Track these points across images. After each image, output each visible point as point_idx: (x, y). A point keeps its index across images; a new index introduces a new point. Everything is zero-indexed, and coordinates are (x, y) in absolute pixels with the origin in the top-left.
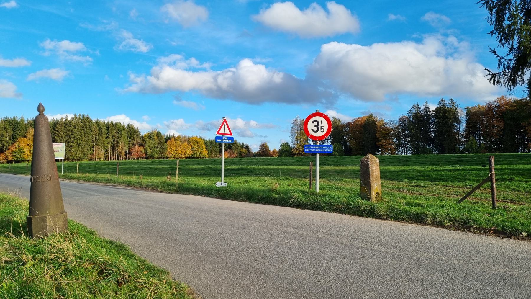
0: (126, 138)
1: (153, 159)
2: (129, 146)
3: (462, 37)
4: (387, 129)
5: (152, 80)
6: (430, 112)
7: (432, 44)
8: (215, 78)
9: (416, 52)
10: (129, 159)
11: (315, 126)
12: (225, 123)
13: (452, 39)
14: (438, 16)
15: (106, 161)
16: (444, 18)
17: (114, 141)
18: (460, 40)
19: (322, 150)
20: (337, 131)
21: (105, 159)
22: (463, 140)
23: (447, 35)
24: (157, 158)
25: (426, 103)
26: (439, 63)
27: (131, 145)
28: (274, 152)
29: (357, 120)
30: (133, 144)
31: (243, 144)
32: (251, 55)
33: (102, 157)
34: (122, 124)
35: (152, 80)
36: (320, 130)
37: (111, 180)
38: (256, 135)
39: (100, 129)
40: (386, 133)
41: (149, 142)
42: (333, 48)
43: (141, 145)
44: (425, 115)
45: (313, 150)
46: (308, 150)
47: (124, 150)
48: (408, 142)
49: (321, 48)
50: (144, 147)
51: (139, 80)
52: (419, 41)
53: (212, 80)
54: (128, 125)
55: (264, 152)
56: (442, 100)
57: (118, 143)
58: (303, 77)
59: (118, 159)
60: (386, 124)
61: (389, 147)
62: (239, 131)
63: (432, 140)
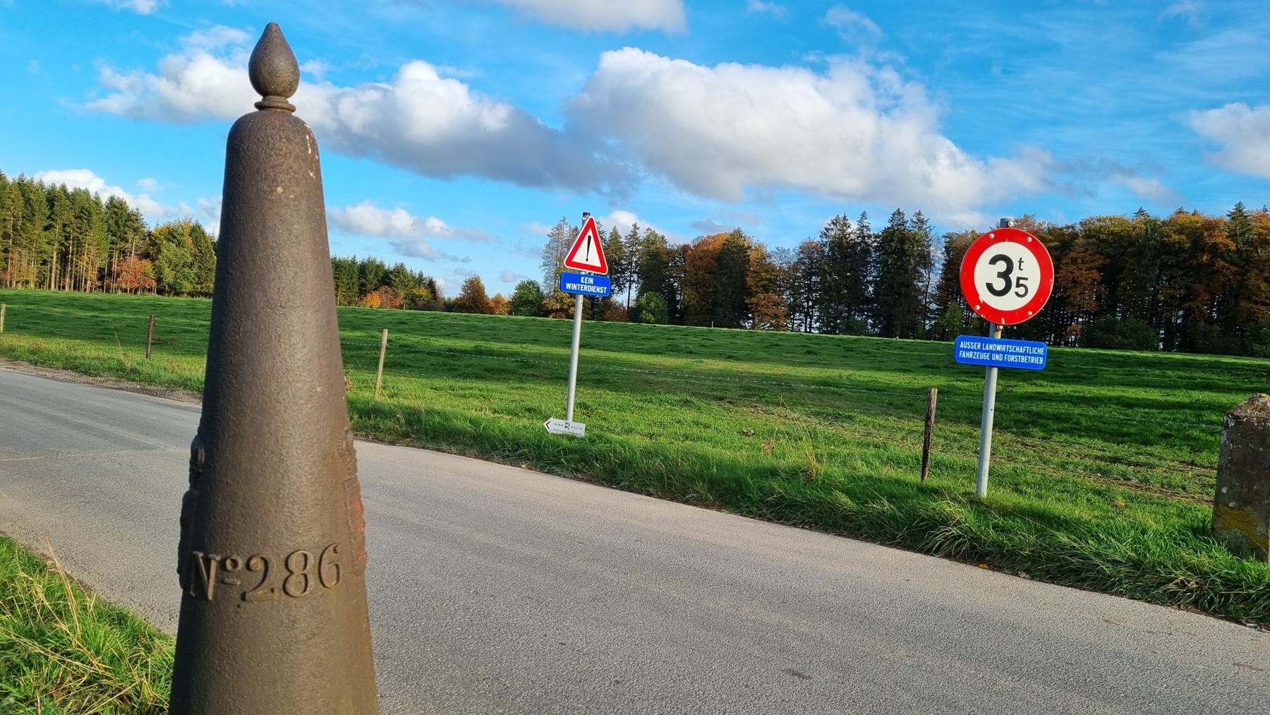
0: (104, 235)
1: (177, 294)
2: (111, 257)
3: (910, 71)
4: (770, 269)
5: (163, 86)
6: (869, 237)
7: (848, 81)
8: (334, 104)
9: (813, 93)
10: (108, 291)
11: (1000, 275)
12: (590, 233)
13: (889, 76)
14: (854, 16)
15: (43, 292)
16: (868, 23)
17: (67, 239)
18: (906, 79)
19: (1012, 358)
20: (655, 265)
21: (40, 284)
22: (933, 306)
23: (879, 66)
24: (191, 294)
25: (864, 216)
26: (864, 123)
27: (116, 254)
28: (497, 301)
29: (705, 243)
30: (123, 252)
31: (421, 275)
32: (441, 55)
33: (33, 279)
34: (92, 194)
35: (163, 86)
36: (1014, 288)
37: (134, 370)
38: (444, 255)
39: (28, 202)
40: (771, 279)
41: (169, 250)
42: (627, 62)
43: (146, 256)
44: (859, 244)
45: (985, 357)
46: (970, 355)
47: (97, 266)
48: (815, 303)
49: (598, 60)
50: (153, 260)
51: (123, 82)
52: (820, 70)
53: (326, 105)
54: (112, 199)
55: (474, 300)
56: (899, 213)
57: (79, 244)
58: (558, 126)
59: (76, 287)
60: (770, 256)
61: (774, 310)
62: (397, 241)
63: (867, 301)
